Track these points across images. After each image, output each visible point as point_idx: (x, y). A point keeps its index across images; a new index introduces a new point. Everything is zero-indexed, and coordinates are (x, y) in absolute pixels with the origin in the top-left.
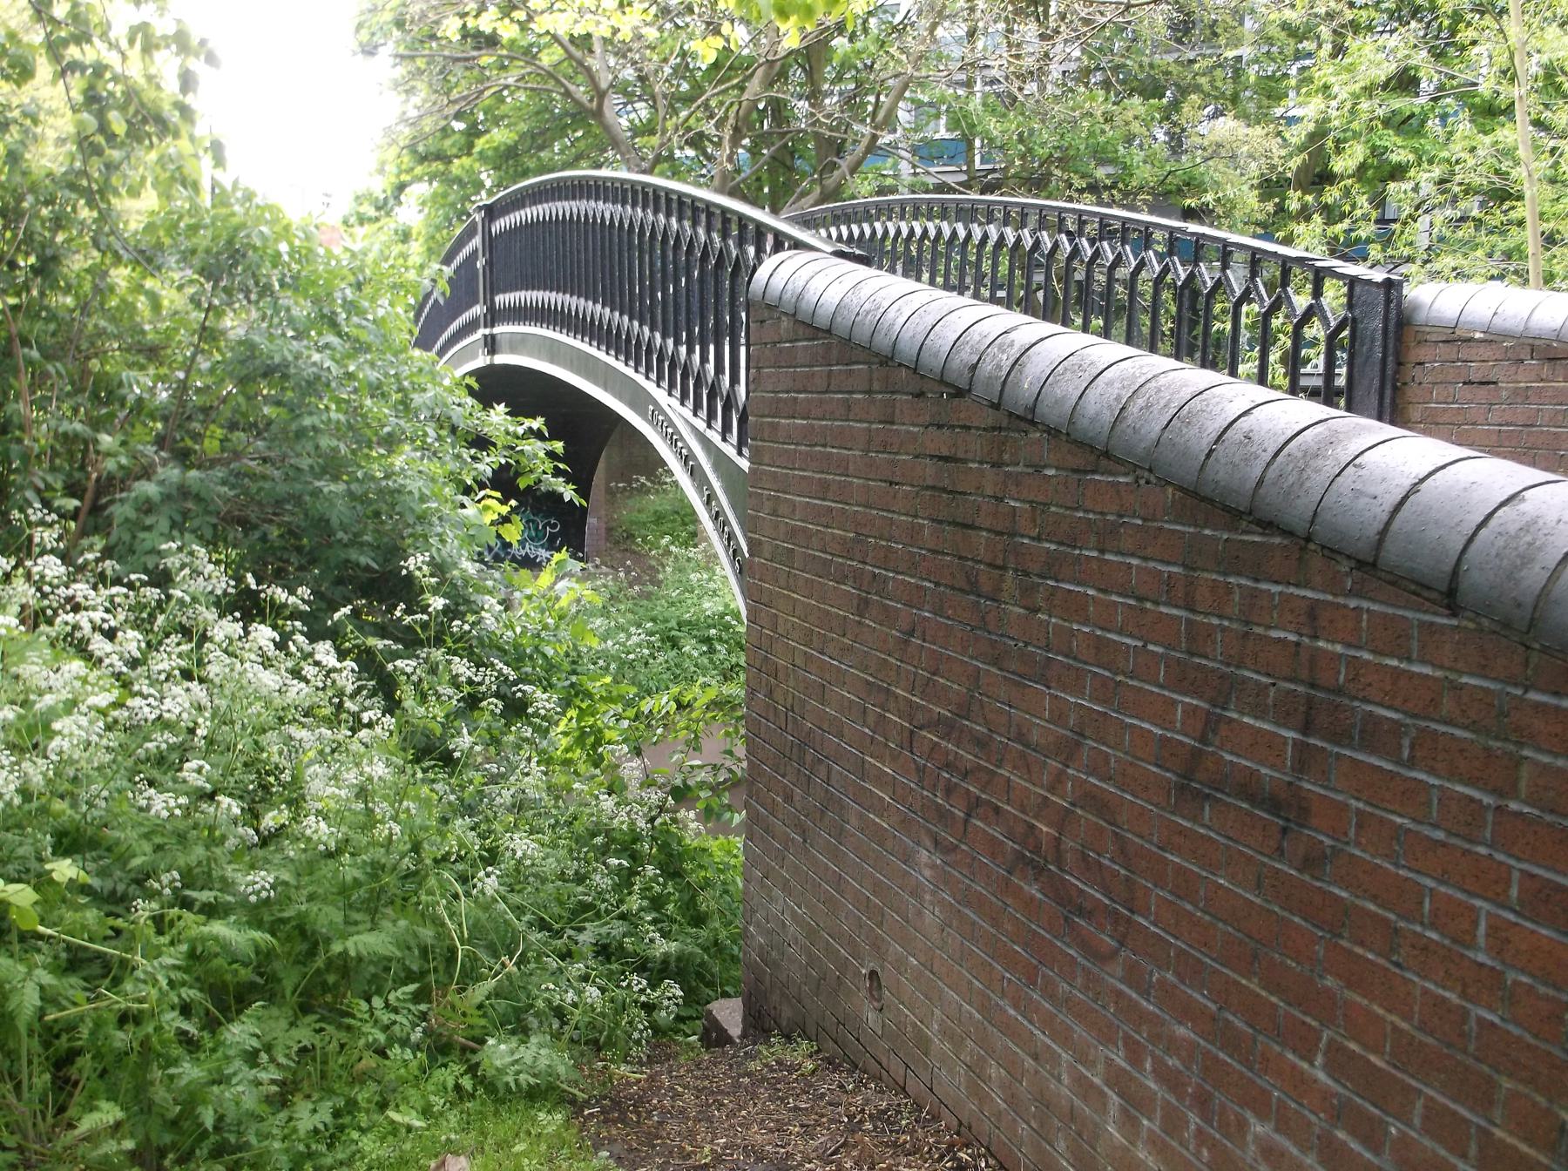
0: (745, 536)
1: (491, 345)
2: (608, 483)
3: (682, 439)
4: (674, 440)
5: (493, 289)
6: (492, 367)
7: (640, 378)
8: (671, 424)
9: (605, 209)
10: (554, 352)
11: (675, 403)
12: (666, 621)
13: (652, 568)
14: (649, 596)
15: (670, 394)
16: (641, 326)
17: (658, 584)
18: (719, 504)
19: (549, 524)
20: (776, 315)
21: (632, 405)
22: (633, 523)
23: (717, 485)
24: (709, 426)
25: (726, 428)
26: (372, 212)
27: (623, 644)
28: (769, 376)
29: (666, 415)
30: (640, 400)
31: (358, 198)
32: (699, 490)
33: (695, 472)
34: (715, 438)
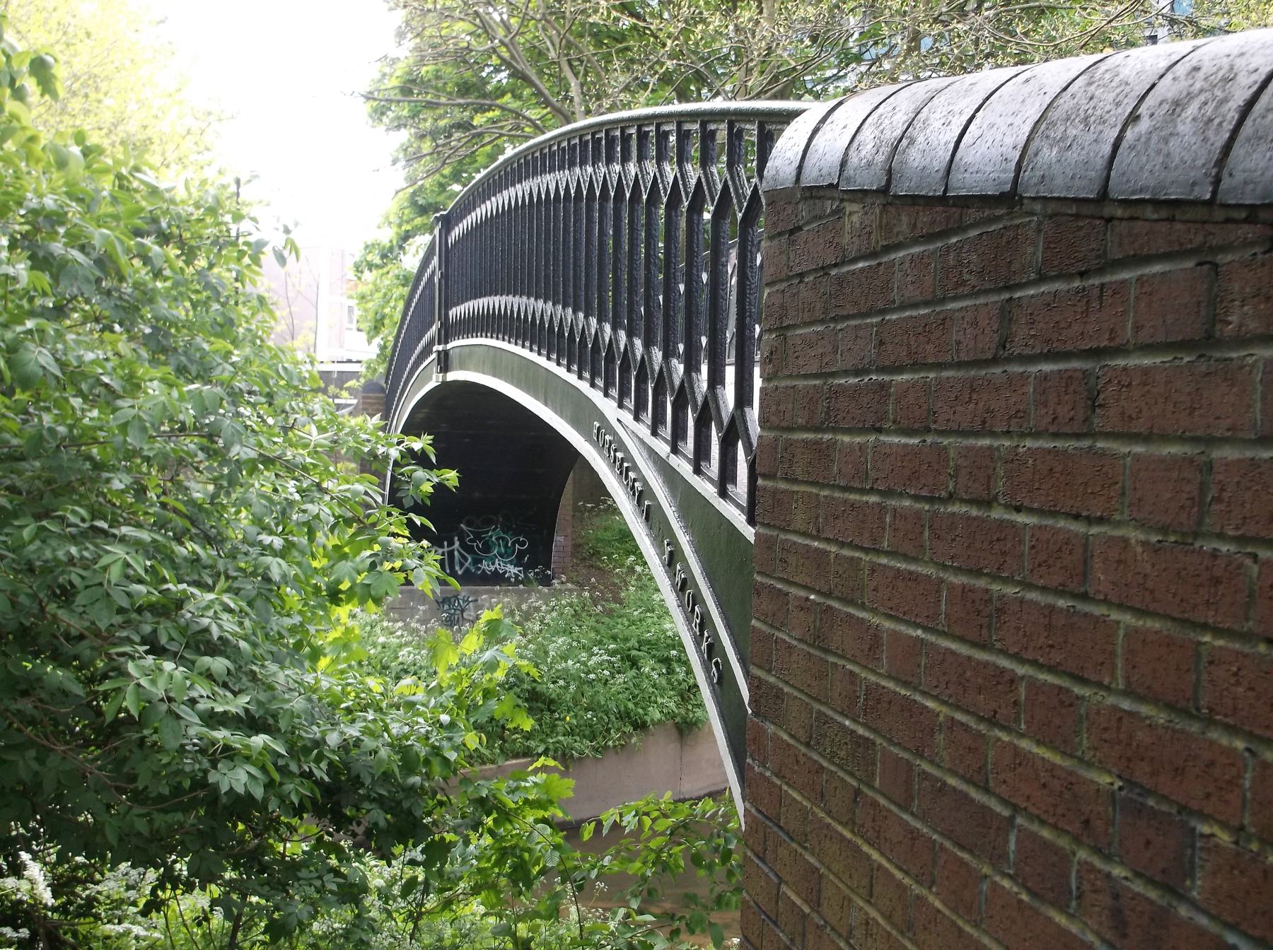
0: (747, 673)
1: (445, 363)
2: (575, 503)
3: (635, 467)
4: (624, 468)
5: (448, 304)
6: (445, 385)
7: (584, 386)
8: (622, 446)
9: (549, 182)
10: (497, 362)
11: (628, 417)
12: (626, 640)
13: (615, 585)
14: (609, 613)
15: (621, 406)
16: (586, 317)
17: (620, 601)
18: (687, 568)
19: (517, 541)
20: (829, 206)
21: (576, 423)
22: (599, 540)
23: (684, 539)
24: (675, 450)
25: (701, 454)
26: (377, 260)
27: (584, 664)
28: (809, 343)
29: (615, 434)
30: (584, 415)
31: (367, 246)
32: (658, 541)
33: (651, 515)
34: (684, 468)
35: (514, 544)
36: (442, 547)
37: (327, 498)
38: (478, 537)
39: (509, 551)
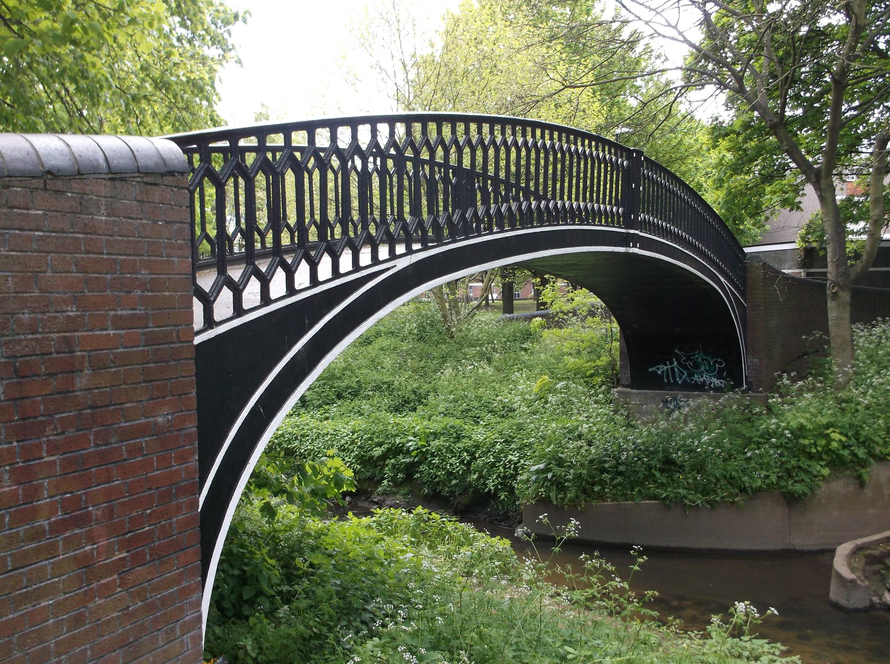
19: (716, 362)
35: (714, 363)
36: (666, 365)
37: (746, 654)
38: (688, 358)
39: (712, 368)
